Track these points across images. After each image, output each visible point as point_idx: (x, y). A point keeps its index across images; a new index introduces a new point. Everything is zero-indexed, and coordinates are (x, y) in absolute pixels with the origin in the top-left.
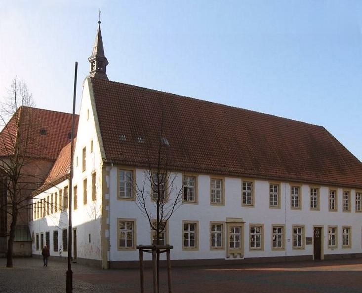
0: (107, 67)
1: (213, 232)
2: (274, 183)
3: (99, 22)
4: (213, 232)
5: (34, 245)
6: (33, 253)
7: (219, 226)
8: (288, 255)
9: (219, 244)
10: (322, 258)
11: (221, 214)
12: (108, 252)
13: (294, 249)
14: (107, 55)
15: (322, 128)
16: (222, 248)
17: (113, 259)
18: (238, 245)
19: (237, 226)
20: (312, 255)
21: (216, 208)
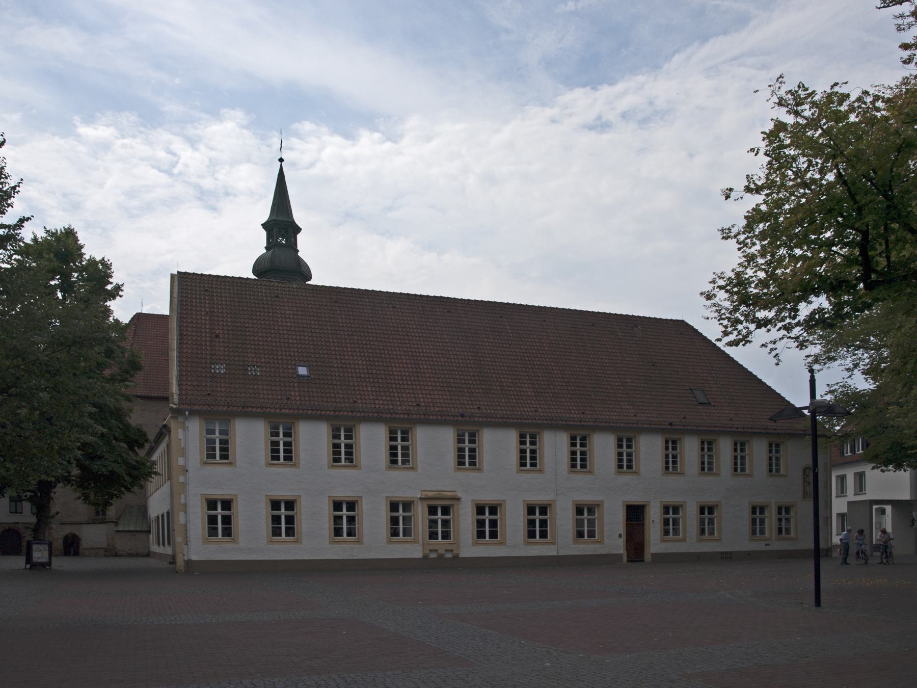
0: (298, 236)
1: (754, 516)
2: (579, 433)
3: (281, 160)
4: (754, 516)
5: (152, 537)
6: (152, 549)
7: (407, 506)
8: (562, 553)
9: (407, 533)
10: (647, 557)
11: (408, 485)
12: (185, 547)
13: (663, 541)
14: (298, 216)
15: (682, 322)
16: (415, 541)
17: (194, 558)
18: (446, 536)
19: (441, 509)
20: (621, 555)
21: (399, 475)
